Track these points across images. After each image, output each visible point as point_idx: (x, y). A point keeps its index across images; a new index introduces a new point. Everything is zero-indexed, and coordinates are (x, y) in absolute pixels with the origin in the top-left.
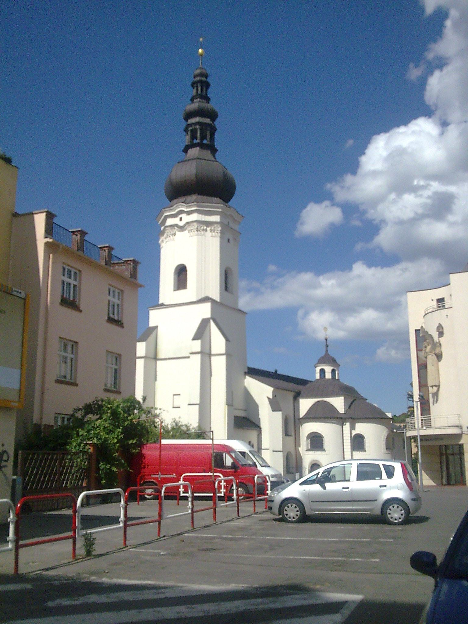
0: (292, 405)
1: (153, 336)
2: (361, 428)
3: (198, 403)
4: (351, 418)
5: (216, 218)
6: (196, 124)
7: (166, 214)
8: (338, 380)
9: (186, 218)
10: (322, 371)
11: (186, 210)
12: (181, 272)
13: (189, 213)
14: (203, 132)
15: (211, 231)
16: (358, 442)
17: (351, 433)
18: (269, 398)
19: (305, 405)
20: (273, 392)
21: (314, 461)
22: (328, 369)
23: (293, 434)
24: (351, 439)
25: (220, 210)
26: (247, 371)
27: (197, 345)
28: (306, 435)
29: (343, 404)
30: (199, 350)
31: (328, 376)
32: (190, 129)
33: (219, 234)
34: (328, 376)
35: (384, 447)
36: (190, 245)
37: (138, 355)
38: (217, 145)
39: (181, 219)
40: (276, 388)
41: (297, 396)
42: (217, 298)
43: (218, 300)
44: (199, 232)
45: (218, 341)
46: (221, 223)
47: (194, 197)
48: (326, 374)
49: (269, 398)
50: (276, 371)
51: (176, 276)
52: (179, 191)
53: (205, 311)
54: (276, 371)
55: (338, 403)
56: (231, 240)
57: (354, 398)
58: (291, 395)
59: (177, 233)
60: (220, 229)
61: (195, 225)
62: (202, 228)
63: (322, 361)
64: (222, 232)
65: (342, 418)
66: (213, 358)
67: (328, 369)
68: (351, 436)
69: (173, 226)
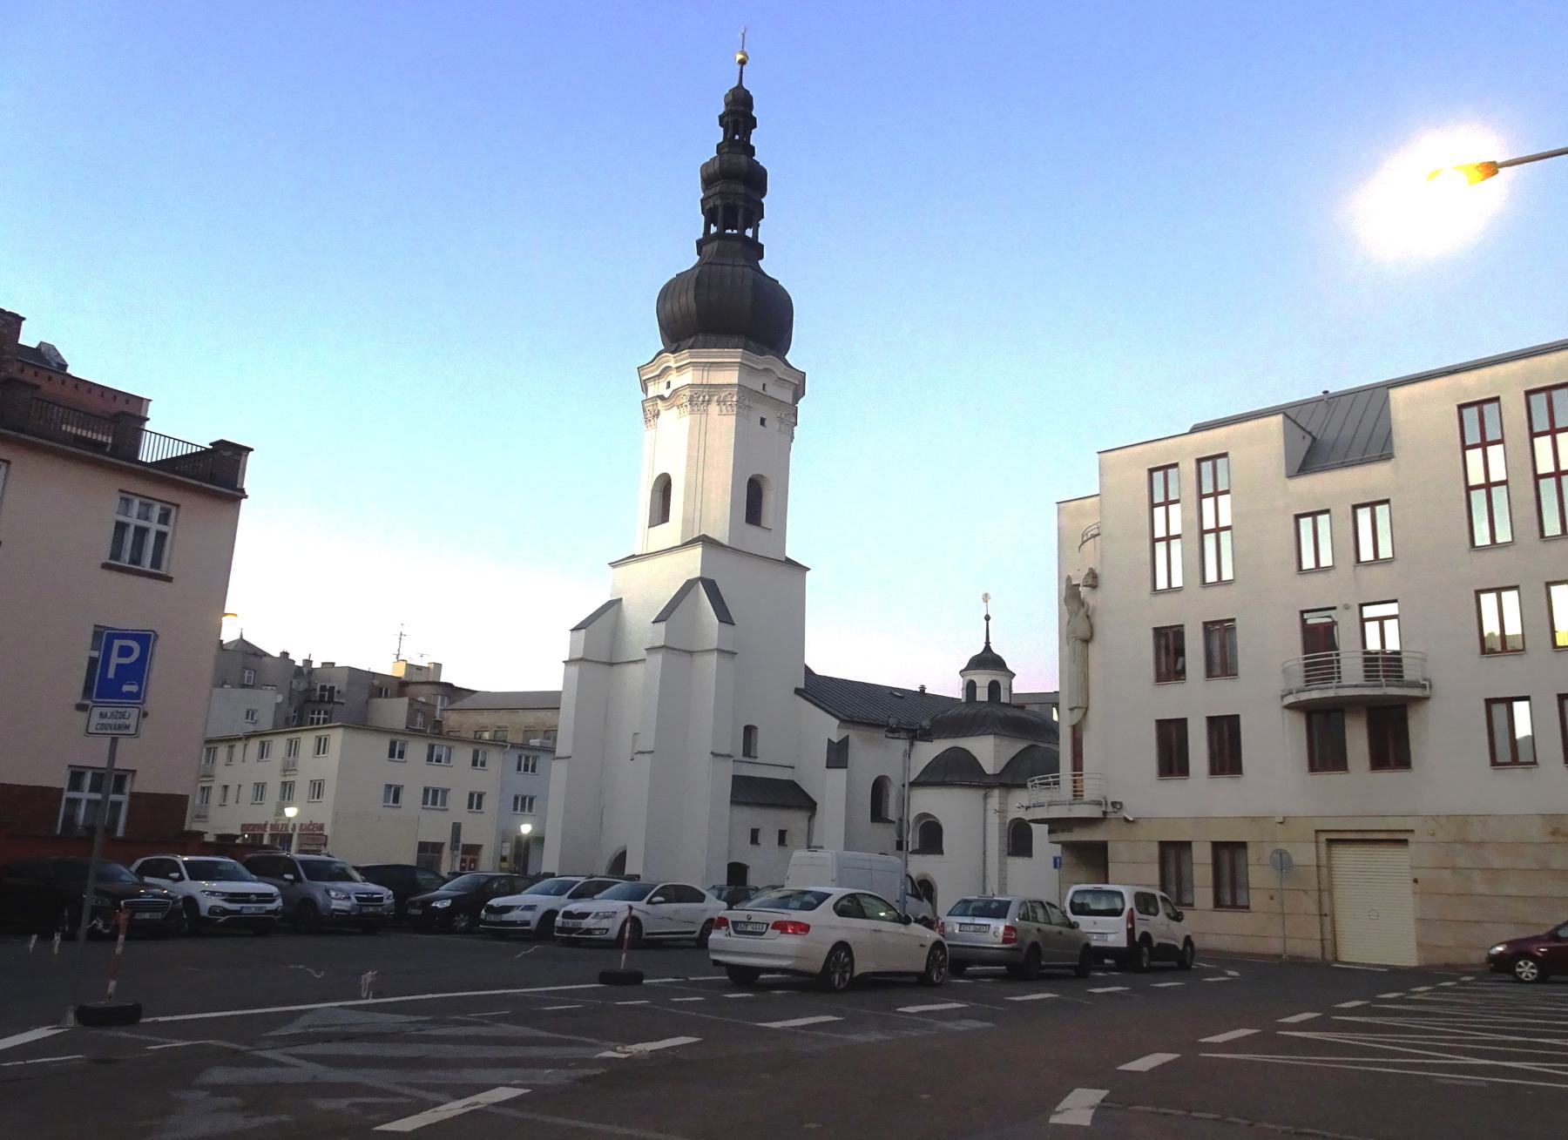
9: (677, 380)
15: (719, 402)
17: (1002, 812)
34: (982, 695)
42: (721, 533)
43: (725, 541)
50: (923, 688)
54: (923, 688)
55: (988, 751)
68: (1002, 823)
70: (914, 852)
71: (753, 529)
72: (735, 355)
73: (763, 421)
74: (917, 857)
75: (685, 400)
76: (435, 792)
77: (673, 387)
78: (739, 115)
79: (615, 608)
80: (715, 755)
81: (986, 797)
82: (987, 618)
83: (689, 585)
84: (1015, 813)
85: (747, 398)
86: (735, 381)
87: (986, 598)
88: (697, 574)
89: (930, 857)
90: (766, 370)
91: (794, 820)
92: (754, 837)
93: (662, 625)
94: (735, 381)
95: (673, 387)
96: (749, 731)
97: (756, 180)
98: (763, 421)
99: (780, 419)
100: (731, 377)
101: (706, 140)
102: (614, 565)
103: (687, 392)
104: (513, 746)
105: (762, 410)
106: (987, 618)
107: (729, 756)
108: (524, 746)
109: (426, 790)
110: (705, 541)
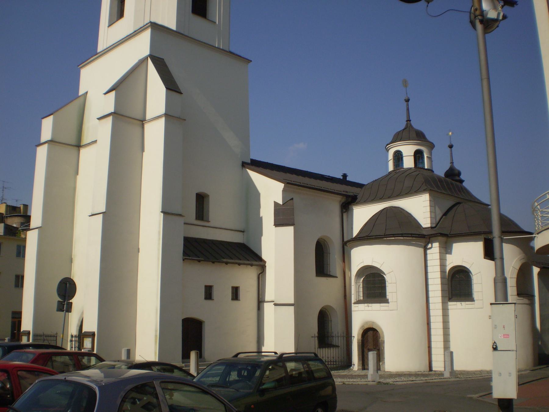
0: (337, 219)
2: (467, 253)
3: (292, 301)
4: (442, 235)
8: (430, 170)
10: (398, 156)
17: (443, 265)
18: (276, 204)
19: (362, 215)
20: (284, 191)
21: (367, 323)
22: (408, 150)
24: (442, 278)
29: (428, 209)
31: (408, 163)
34: (408, 163)
37: (43, 140)
40: (288, 184)
41: (348, 204)
42: (170, 21)
43: (173, 27)
48: (405, 159)
49: (276, 204)
50: (345, 176)
53: (142, 46)
54: (345, 176)
55: (419, 207)
57: (457, 200)
58: (334, 205)
63: (399, 137)
65: (422, 236)
66: (147, 126)
67: (408, 150)
68: (443, 271)
70: (358, 302)
71: (198, 20)
74: (362, 306)
80: (98, 119)
81: (426, 249)
84: (452, 261)
87: (405, 83)
89: (376, 306)
91: (245, 277)
92: (209, 293)
102: (105, 94)
110: (155, 27)
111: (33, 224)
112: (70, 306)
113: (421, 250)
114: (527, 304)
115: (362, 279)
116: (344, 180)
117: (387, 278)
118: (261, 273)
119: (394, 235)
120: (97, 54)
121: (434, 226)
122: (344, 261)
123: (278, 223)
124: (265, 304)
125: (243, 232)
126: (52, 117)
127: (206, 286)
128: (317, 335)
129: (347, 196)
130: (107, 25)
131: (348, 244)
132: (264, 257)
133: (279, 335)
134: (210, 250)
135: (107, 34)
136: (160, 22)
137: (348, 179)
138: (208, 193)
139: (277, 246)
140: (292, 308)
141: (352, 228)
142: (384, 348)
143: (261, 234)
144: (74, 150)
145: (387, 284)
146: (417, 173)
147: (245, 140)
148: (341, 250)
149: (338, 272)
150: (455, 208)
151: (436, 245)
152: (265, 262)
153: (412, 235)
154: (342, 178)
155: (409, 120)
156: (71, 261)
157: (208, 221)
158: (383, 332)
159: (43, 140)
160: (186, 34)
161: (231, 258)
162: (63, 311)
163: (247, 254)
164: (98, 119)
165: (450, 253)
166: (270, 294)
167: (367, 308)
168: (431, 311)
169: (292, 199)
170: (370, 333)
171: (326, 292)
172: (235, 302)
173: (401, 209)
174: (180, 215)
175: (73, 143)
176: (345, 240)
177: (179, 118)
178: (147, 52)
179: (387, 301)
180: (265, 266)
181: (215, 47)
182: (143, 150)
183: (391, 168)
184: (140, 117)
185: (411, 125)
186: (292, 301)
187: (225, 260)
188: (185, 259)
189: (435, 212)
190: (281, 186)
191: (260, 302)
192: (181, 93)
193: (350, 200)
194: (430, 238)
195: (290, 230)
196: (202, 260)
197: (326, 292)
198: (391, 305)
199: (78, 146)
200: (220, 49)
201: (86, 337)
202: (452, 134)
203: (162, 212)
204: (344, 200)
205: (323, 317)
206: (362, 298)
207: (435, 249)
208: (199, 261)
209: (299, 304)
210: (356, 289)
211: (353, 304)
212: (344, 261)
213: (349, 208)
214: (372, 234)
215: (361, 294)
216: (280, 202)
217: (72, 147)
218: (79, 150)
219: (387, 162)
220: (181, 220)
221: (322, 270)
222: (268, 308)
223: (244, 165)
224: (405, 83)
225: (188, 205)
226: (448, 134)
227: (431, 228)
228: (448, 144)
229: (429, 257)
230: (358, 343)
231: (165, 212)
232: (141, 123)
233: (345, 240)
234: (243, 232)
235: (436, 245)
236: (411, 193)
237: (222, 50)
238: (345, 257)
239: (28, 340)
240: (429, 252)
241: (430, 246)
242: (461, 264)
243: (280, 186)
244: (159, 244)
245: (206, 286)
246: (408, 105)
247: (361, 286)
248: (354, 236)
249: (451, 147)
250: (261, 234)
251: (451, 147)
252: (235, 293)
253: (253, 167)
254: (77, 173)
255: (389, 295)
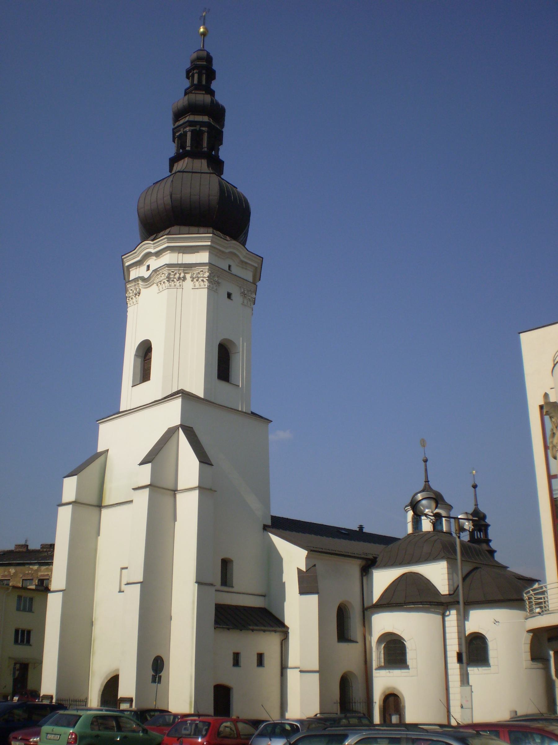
1: (96, 465)
2: (480, 620)
5: (203, 257)
6: (202, 124)
7: (127, 264)
9: (154, 263)
11: (153, 251)
12: (145, 350)
13: (158, 254)
14: (201, 130)
15: (193, 279)
16: (475, 650)
18: (299, 571)
19: (383, 579)
20: (307, 558)
21: (388, 688)
23: (359, 638)
25: (209, 243)
26: (269, 523)
27: (145, 475)
28: (376, 641)
29: (446, 576)
30: (148, 482)
32: (177, 134)
33: (206, 283)
35: (527, 656)
36: (168, 308)
37: (65, 500)
38: (224, 153)
39: (148, 267)
40: (313, 551)
41: (368, 566)
42: (199, 390)
43: (201, 394)
44: (172, 284)
45: (188, 467)
46: (210, 264)
47: (175, 228)
49: (299, 571)
50: (361, 528)
51: (139, 360)
52: (154, 225)
53: (172, 414)
54: (361, 528)
56: (236, 296)
57: (475, 565)
58: (354, 568)
59: (143, 291)
60: (207, 274)
61: (166, 271)
62: (177, 275)
64: (210, 279)
66: (179, 496)
69: (136, 280)
70: (380, 668)
72: (205, 239)
73: (229, 295)
74: (383, 672)
75: (163, 277)
76: (23, 631)
77: (152, 269)
78: (203, 71)
79: (102, 458)
81: (444, 616)
82: (426, 461)
83: (171, 433)
84: (471, 627)
85: (217, 277)
86: (206, 261)
87: (423, 443)
88: (179, 423)
90: (231, 253)
91: (268, 643)
92: (236, 660)
93: (149, 466)
94: (206, 261)
95: (152, 269)
96: (226, 564)
97: (217, 113)
98: (229, 295)
99: (244, 295)
100: (203, 257)
101: (175, 90)
102: (134, 489)
103: (166, 271)
104: (14, 587)
105: (227, 286)
106: (426, 461)
107: (211, 585)
108: (24, 588)
109: (17, 631)
111: (54, 586)
112: (160, 677)
113: (439, 617)
114: (542, 668)
115: (383, 645)
116: (359, 535)
117: (407, 644)
118: (284, 639)
119: (413, 603)
120: (120, 413)
121: (452, 592)
122: (364, 625)
123: (303, 591)
124: (288, 670)
125: (264, 596)
126: (76, 477)
127: (234, 653)
128: (339, 701)
129: (367, 559)
130: (131, 384)
131: (369, 610)
132: (287, 623)
133: (303, 700)
134: (240, 617)
135: (131, 394)
136: (187, 389)
137: (364, 530)
138: (232, 558)
139: (301, 613)
140: (317, 675)
141: (372, 592)
142: (405, 713)
143: (283, 599)
144: (96, 510)
145: (408, 650)
146: (436, 537)
147: (265, 500)
148: (362, 614)
149: (359, 637)
150: (473, 574)
151: (454, 612)
152: (288, 628)
153: (431, 603)
154: (358, 529)
155: (427, 481)
156: (92, 624)
157: (233, 587)
158: (403, 698)
159: (65, 500)
160: (213, 400)
161: (257, 625)
162: (155, 683)
163: (270, 619)
164: (133, 489)
165: (468, 620)
166: (293, 659)
167: (388, 674)
168: (449, 677)
169: (315, 565)
170: (391, 699)
171: (348, 657)
172: (261, 669)
173: (421, 575)
174: (211, 585)
175: (94, 503)
176: (365, 606)
177: (211, 489)
178: (178, 422)
179: (407, 667)
180: (288, 633)
181: (238, 411)
182: (175, 519)
183: (410, 530)
184: (171, 487)
185: (429, 486)
186: (316, 667)
187: (251, 627)
188: (217, 627)
189: (453, 580)
190: (304, 553)
191: (284, 667)
192: (212, 465)
193: (370, 562)
194: (447, 606)
195: (314, 599)
196: (232, 629)
197: (348, 657)
198: (411, 671)
199: (100, 506)
200: (243, 412)
201: (123, 703)
202: (476, 472)
203: (196, 582)
204: (363, 563)
205: (345, 682)
206: (383, 664)
207: (452, 617)
208: (228, 629)
209: (323, 671)
210: (377, 655)
211: (374, 671)
212: (364, 625)
213: (368, 571)
214: (393, 600)
215: (382, 660)
216: (304, 569)
217: (94, 508)
218: (101, 511)
219: (406, 523)
220: (212, 589)
221: (343, 635)
222: (293, 676)
223: (265, 528)
224: (423, 443)
225: (217, 571)
226: (472, 473)
227: (449, 595)
228: (472, 483)
229: (447, 624)
230: (380, 709)
231: (200, 583)
232: (173, 492)
233: (366, 606)
234: (264, 596)
235: (454, 612)
236: (430, 560)
237: (245, 413)
238: (366, 623)
239: (131, 706)
240: (447, 619)
241: (448, 613)
242: (477, 631)
243: (304, 553)
244: (193, 613)
245: (234, 653)
246: (426, 466)
247: (382, 652)
248: (374, 602)
249: (475, 487)
250: (284, 600)
251: (475, 487)
252: (260, 660)
253: (274, 530)
254: (98, 534)
255: (409, 661)
